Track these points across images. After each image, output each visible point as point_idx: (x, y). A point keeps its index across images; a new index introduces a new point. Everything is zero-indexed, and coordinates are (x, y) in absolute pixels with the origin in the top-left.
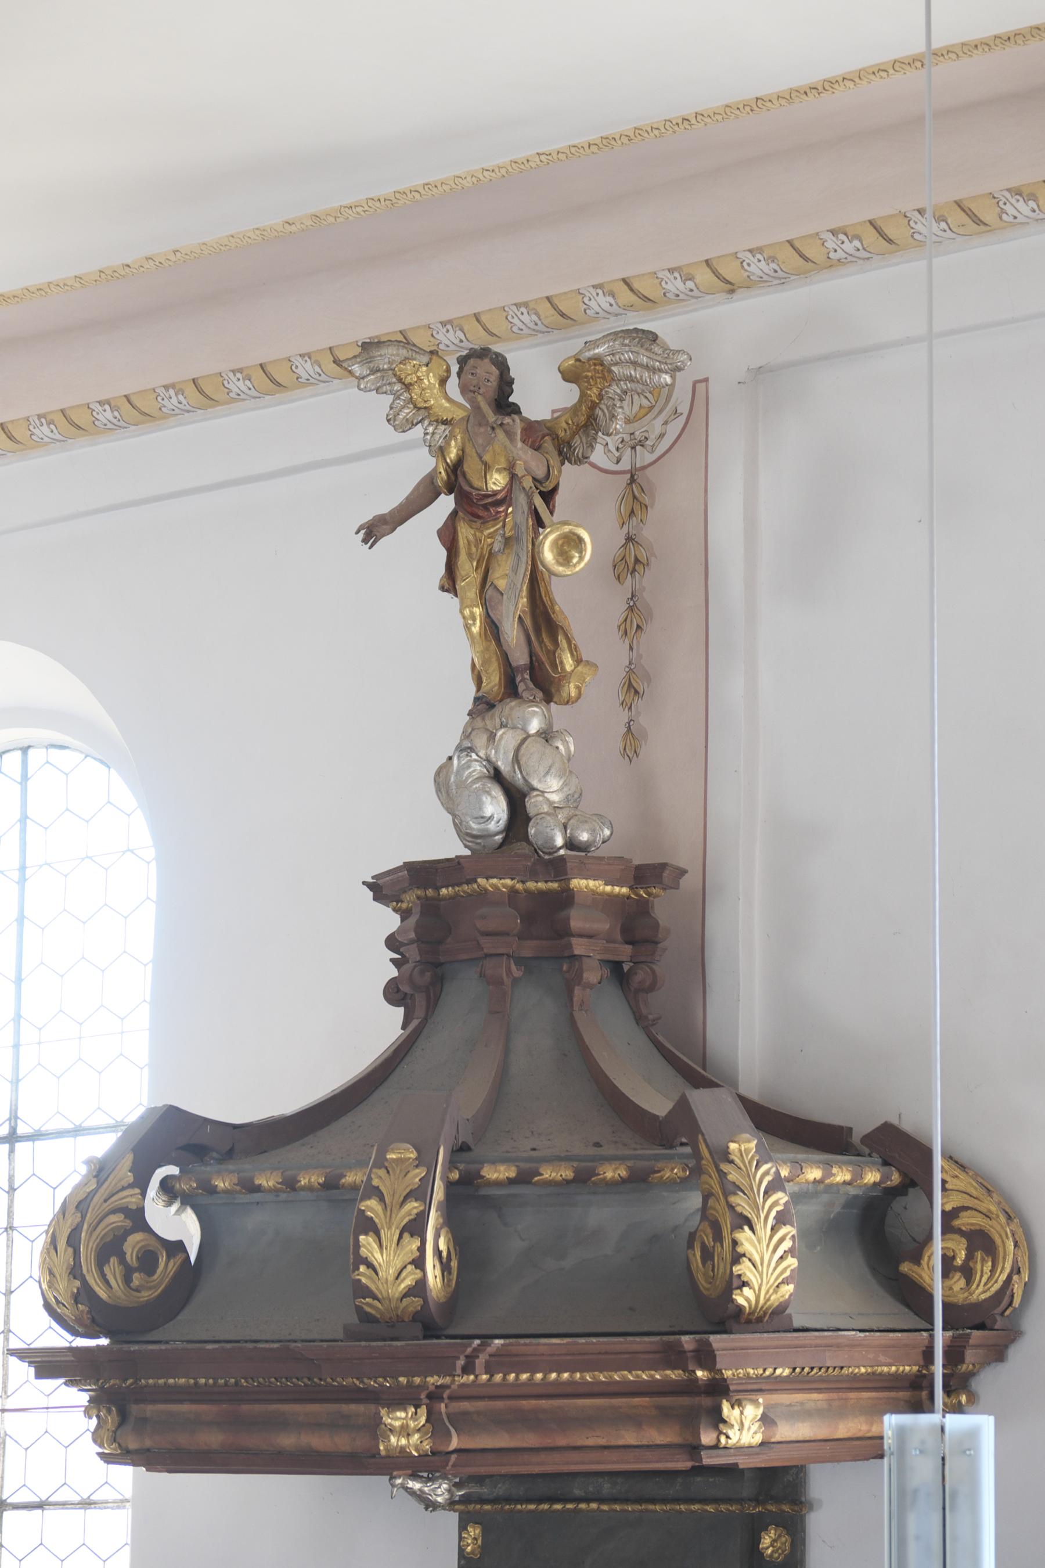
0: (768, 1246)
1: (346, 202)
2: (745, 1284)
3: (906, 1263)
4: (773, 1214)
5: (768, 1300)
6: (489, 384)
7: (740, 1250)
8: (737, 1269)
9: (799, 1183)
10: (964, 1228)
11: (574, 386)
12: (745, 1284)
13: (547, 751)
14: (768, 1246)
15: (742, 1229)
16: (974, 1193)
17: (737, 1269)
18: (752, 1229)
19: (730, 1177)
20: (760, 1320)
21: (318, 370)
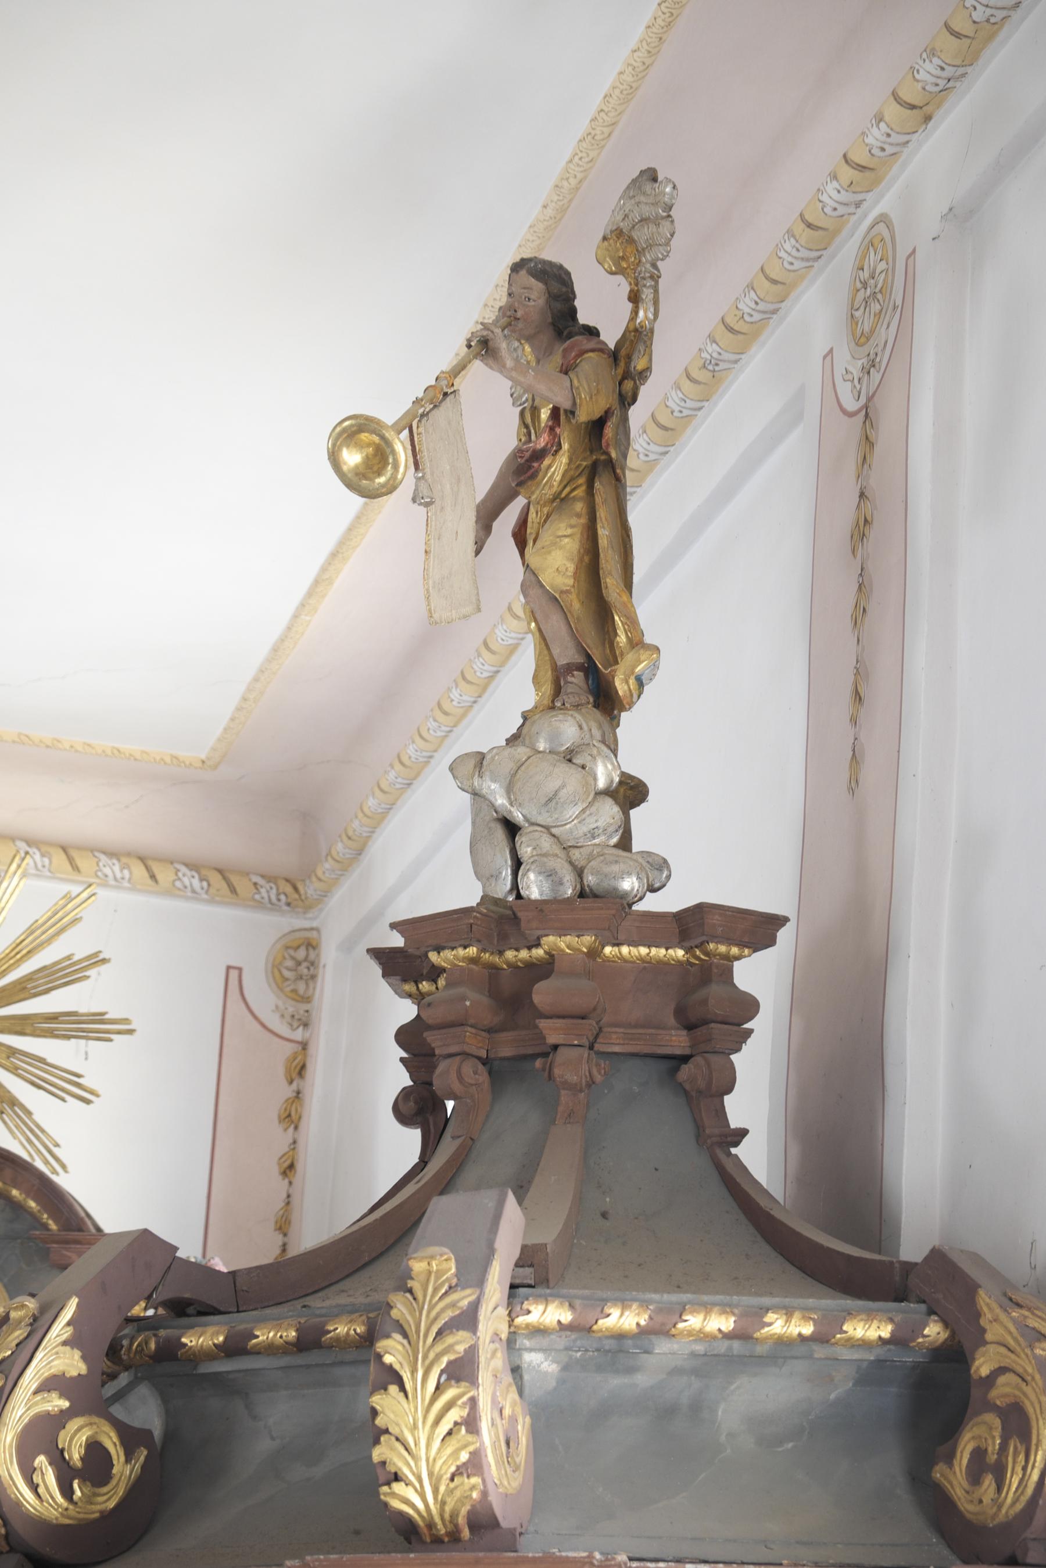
0: (425, 1418)
1: (567, 157)
2: (397, 1478)
3: (933, 1475)
4: (444, 1361)
5: (443, 1503)
6: (532, 303)
7: (379, 1421)
8: (377, 1454)
9: (459, 1308)
10: (998, 1403)
11: (620, 278)
12: (397, 1478)
13: (556, 770)
14: (425, 1418)
15: (386, 1389)
16: (1011, 1343)
17: (377, 1454)
18: (402, 1388)
19: (394, 1314)
20: (454, 1536)
21: (681, 395)
